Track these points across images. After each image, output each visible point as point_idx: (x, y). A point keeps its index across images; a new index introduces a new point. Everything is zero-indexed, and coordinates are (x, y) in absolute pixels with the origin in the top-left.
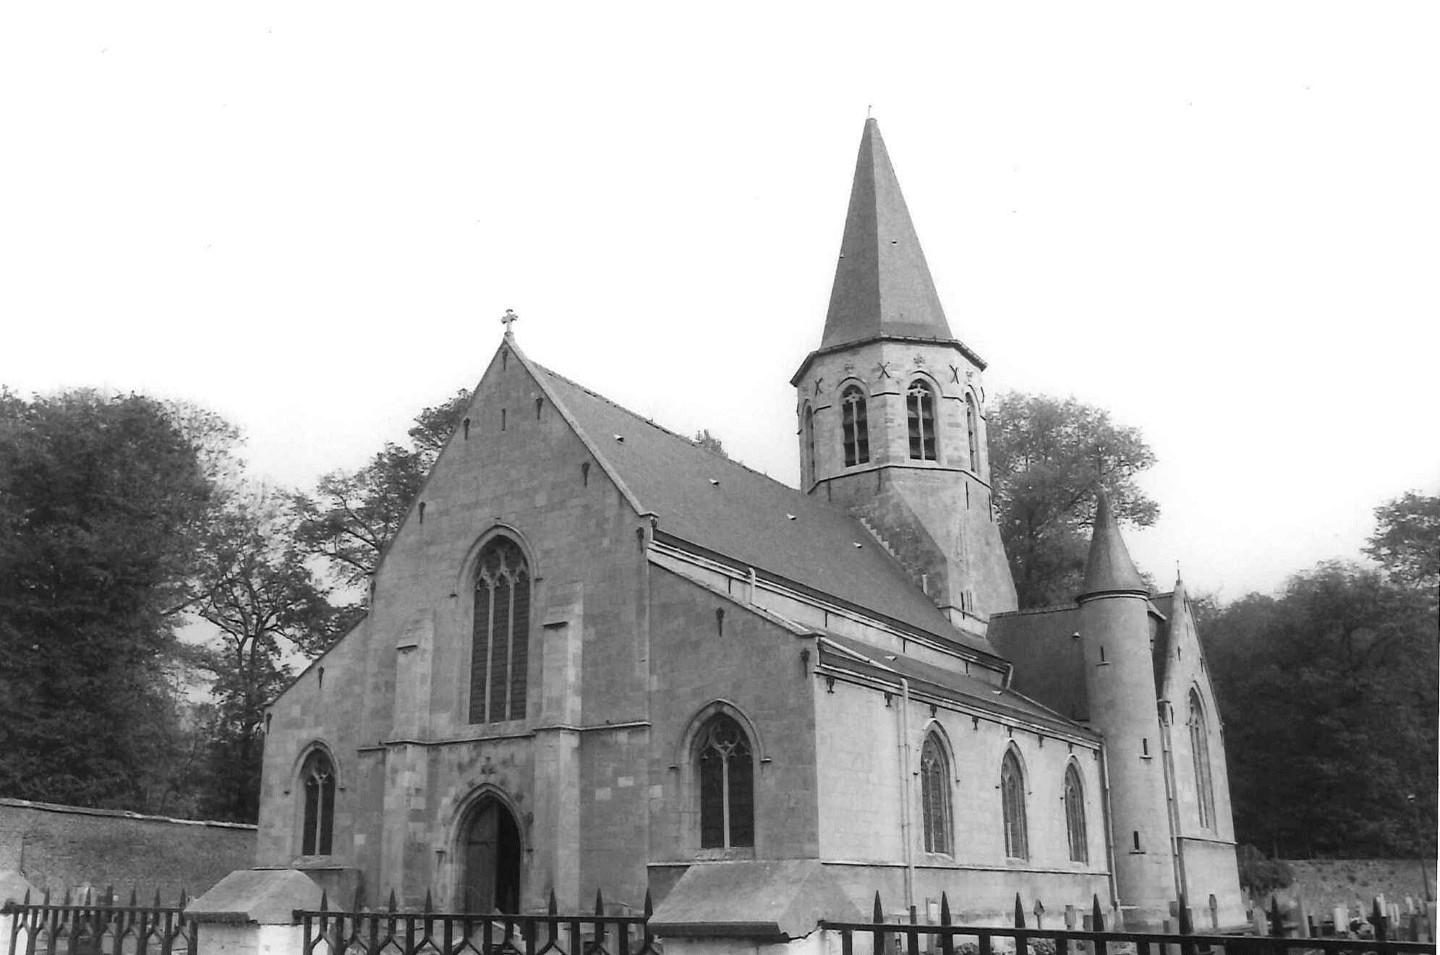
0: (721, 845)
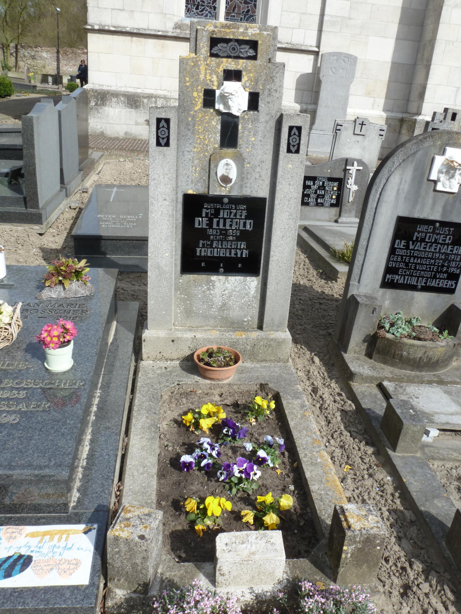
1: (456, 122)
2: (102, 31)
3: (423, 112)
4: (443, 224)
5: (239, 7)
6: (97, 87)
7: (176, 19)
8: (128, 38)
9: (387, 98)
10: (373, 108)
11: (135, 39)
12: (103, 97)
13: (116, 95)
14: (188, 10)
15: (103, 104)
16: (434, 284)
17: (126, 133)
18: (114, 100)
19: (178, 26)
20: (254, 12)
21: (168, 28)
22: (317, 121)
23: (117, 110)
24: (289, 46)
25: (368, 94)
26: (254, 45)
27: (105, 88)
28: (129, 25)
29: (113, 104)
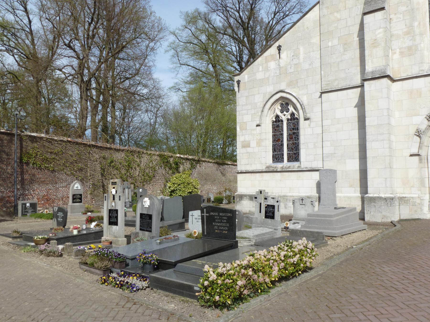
0: (283, 161)
1: (262, 194)
2: (241, 173)
3: (369, 192)
4: (147, 214)
5: (292, 156)
6: (240, 193)
7: (268, 165)
8: (250, 174)
9: (361, 187)
10: (355, 193)
11: (252, 174)
12: (241, 197)
13: (246, 196)
14: (273, 160)
15: (242, 200)
16: (147, 229)
17: (249, 211)
18: (245, 198)
19: (268, 167)
20: (298, 157)
21: (264, 168)
22: (321, 201)
23: (246, 202)
24: (311, 169)
25: (351, 186)
26: (116, 182)
27: (242, 193)
28: (250, 169)
29: (245, 199)
